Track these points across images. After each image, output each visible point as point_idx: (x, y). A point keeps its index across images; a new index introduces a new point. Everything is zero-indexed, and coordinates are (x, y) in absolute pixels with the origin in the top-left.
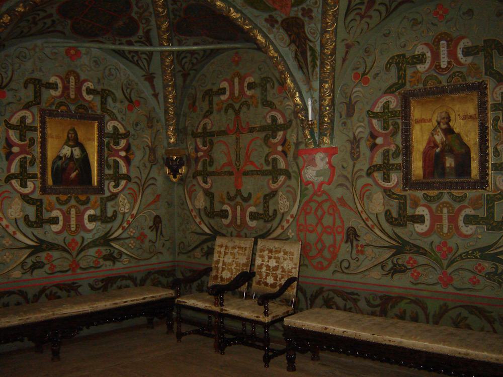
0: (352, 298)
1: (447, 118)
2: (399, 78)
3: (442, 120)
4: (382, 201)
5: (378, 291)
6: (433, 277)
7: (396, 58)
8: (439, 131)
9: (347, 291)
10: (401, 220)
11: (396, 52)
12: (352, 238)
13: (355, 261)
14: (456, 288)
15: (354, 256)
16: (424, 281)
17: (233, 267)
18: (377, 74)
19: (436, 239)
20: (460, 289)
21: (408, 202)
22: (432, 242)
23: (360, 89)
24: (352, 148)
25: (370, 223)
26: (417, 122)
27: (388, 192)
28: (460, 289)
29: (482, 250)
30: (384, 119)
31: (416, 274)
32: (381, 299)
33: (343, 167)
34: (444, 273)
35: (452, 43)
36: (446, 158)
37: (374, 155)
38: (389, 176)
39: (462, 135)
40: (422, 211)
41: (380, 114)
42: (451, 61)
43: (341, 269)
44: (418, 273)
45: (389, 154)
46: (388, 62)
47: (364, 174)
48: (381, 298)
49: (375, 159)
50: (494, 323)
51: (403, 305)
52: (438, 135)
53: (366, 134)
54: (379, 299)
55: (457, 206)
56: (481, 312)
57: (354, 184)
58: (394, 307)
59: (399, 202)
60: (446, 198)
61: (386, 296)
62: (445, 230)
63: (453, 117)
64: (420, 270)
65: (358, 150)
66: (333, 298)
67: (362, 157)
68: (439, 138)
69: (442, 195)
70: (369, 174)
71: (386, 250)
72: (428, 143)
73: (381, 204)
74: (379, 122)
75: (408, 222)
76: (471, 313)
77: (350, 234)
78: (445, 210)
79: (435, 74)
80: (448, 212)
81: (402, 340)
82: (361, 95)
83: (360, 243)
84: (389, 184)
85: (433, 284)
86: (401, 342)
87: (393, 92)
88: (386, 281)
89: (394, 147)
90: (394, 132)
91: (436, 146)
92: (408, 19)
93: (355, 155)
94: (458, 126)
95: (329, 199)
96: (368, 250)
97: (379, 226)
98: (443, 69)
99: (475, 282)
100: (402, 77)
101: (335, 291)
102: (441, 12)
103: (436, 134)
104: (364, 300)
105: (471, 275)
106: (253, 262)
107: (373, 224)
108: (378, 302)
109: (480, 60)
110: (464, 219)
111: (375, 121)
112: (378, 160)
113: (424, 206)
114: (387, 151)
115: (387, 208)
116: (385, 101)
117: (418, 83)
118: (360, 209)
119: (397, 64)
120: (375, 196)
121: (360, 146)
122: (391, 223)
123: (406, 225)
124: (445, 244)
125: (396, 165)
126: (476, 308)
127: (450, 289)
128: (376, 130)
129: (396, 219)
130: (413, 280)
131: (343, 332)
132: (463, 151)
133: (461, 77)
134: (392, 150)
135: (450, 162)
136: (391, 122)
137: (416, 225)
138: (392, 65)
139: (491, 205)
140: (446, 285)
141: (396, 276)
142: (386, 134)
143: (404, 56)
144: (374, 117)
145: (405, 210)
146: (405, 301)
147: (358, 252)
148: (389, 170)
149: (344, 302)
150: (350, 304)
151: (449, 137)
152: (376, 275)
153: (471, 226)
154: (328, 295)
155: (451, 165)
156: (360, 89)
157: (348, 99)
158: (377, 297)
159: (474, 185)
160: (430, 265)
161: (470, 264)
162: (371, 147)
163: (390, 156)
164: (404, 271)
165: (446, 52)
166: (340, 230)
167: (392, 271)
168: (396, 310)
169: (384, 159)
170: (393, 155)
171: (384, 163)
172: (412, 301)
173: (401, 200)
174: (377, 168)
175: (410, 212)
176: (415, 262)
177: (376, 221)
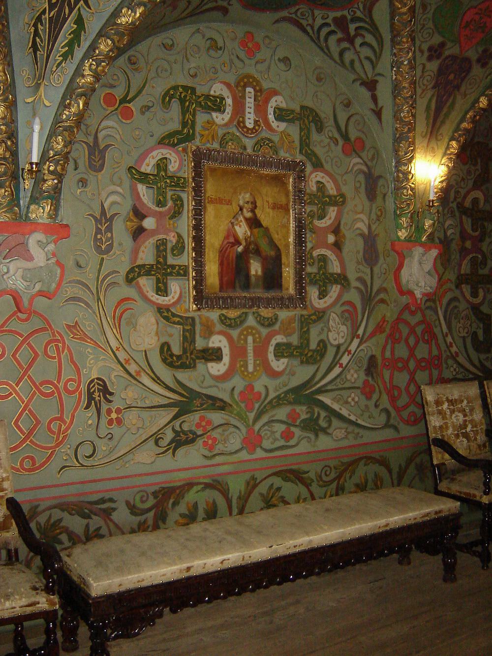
0: (100, 509)
1: (252, 203)
2: (184, 124)
3: (246, 205)
4: (155, 327)
5: (147, 485)
6: (235, 441)
7: (181, 90)
8: (241, 221)
9: (93, 500)
10: (187, 358)
11: (183, 80)
12: (97, 398)
13: (106, 440)
14: (266, 451)
15: (103, 432)
16: (227, 452)
17: (469, 429)
18: (148, 108)
19: (238, 383)
20: (271, 451)
21: (198, 328)
22: (233, 389)
23: (115, 125)
24: (98, 231)
25: (133, 368)
26: (212, 201)
27: (164, 313)
28: (271, 451)
29: (296, 390)
30: (158, 188)
31: (210, 442)
32: (155, 497)
33: (79, 266)
34: (250, 431)
35: (263, 97)
36: (252, 261)
37: (140, 247)
38: (166, 285)
39: (272, 230)
40: (217, 341)
41: (151, 177)
42: (259, 121)
43: (77, 460)
44: (215, 440)
45: (166, 249)
46: (167, 93)
47: (121, 279)
48: (155, 494)
49: (141, 255)
50: (311, 486)
51: (191, 496)
52: (240, 226)
53: (126, 207)
54: (151, 497)
55: (264, 331)
56: (295, 475)
57: (102, 298)
58: (178, 503)
59: (184, 329)
60: (251, 321)
61: (164, 488)
62: (251, 368)
63: (259, 203)
64: (215, 434)
65: (109, 235)
66: (60, 520)
67: (116, 250)
68: (242, 230)
69: (246, 316)
70: (130, 279)
71: (162, 412)
72: (227, 237)
73: (153, 333)
74: (151, 191)
75: (197, 361)
76: (286, 479)
77: (94, 391)
78: (250, 339)
79: (238, 134)
80: (254, 341)
81: (311, 538)
82: (118, 137)
83: (114, 407)
84: (166, 298)
85: (236, 452)
86: (311, 541)
87: (174, 145)
88: (167, 462)
89: (174, 237)
90: (175, 212)
91: (237, 242)
92: (204, 36)
93: (103, 248)
94: (266, 217)
95: (47, 326)
96: (131, 417)
97: (149, 372)
98: (248, 129)
99: (287, 435)
100: (188, 124)
101: (64, 507)
102: (250, 45)
103: (237, 225)
104: (124, 504)
105: (283, 427)
106: (487, 411)
107: (138, 369)
108: (151, 502)
109: (294, 131)
110: (275, 350)
111: (141, 188)
112: (147, 255)
113: (220, 333)
114: (164, 242)
115: (163, 340)
116: (160, 157)
117: (213, 139)
118: (114, 344)
119: (182, 101)
120: (142, 320)
121: (114, 227)
122: (171, 365)
123: (195, 367)
124: (250, 388)
125: (177, 267)
126: (291, 471)
127: (259, 454)
128: (143, 204)
129: (179, 357)
130: (207, 453)
131: (222, 563)
132: (273, 253)
133: (271, 147)
134: (172, 242)
135: (256, 268)
136: (170, 194)
137: (210, 365)
138: (173, 100)
139: (306, 329)
140: (252, 450)
141: (181, 452)
142: (160, 213)
143: (193, 90)
144: (141, 181)
145: (193, 341)
146: (195, 488)
147: (110, 422)
148: (167, 274)
149: (85, 521)
150: (96, 522)
151: (256, 231)
152: (146, 458)
153: (282, 360)
154: (50, 517)
155: (256, 272)
156: (115, 125)
157: (93, 137)
158: (148, 495)
159: (284, 303)
160: (232, 423)
161: (282, 413)
162: (135, 232)
163: (169, 251)
164: (193, 441)
165: (252, 105)
166: (71, 386)
167: (174, 444)
168: (182, 508)
169: (158, 256)
170: (173, 250)
171: (158, 262)
172: (207, 486)
173: (187, 325)
174: (146, 270)
175: (200, 344)
176: (209, 422)
177: (144, 365)
